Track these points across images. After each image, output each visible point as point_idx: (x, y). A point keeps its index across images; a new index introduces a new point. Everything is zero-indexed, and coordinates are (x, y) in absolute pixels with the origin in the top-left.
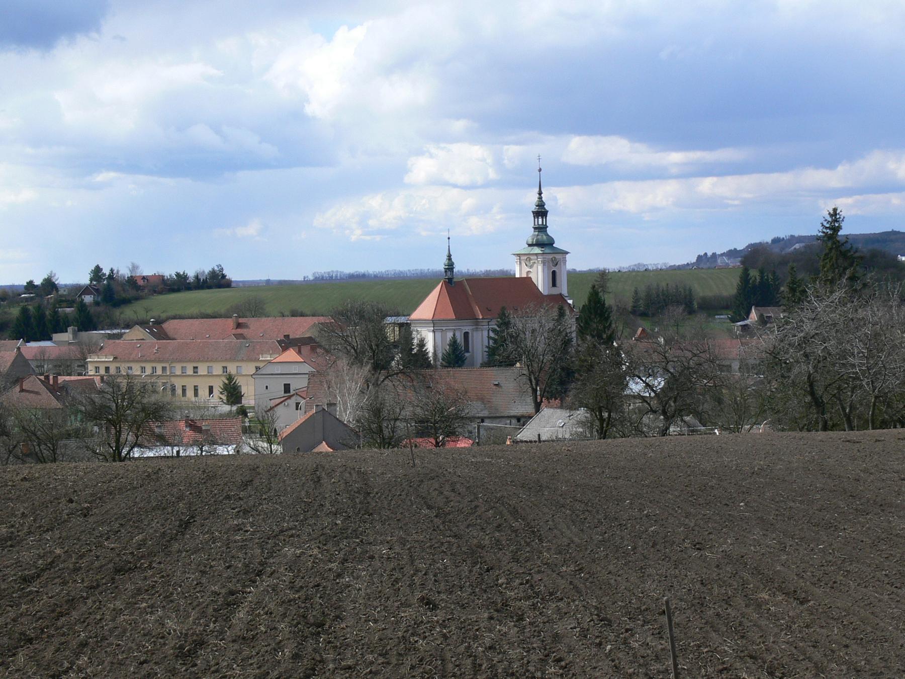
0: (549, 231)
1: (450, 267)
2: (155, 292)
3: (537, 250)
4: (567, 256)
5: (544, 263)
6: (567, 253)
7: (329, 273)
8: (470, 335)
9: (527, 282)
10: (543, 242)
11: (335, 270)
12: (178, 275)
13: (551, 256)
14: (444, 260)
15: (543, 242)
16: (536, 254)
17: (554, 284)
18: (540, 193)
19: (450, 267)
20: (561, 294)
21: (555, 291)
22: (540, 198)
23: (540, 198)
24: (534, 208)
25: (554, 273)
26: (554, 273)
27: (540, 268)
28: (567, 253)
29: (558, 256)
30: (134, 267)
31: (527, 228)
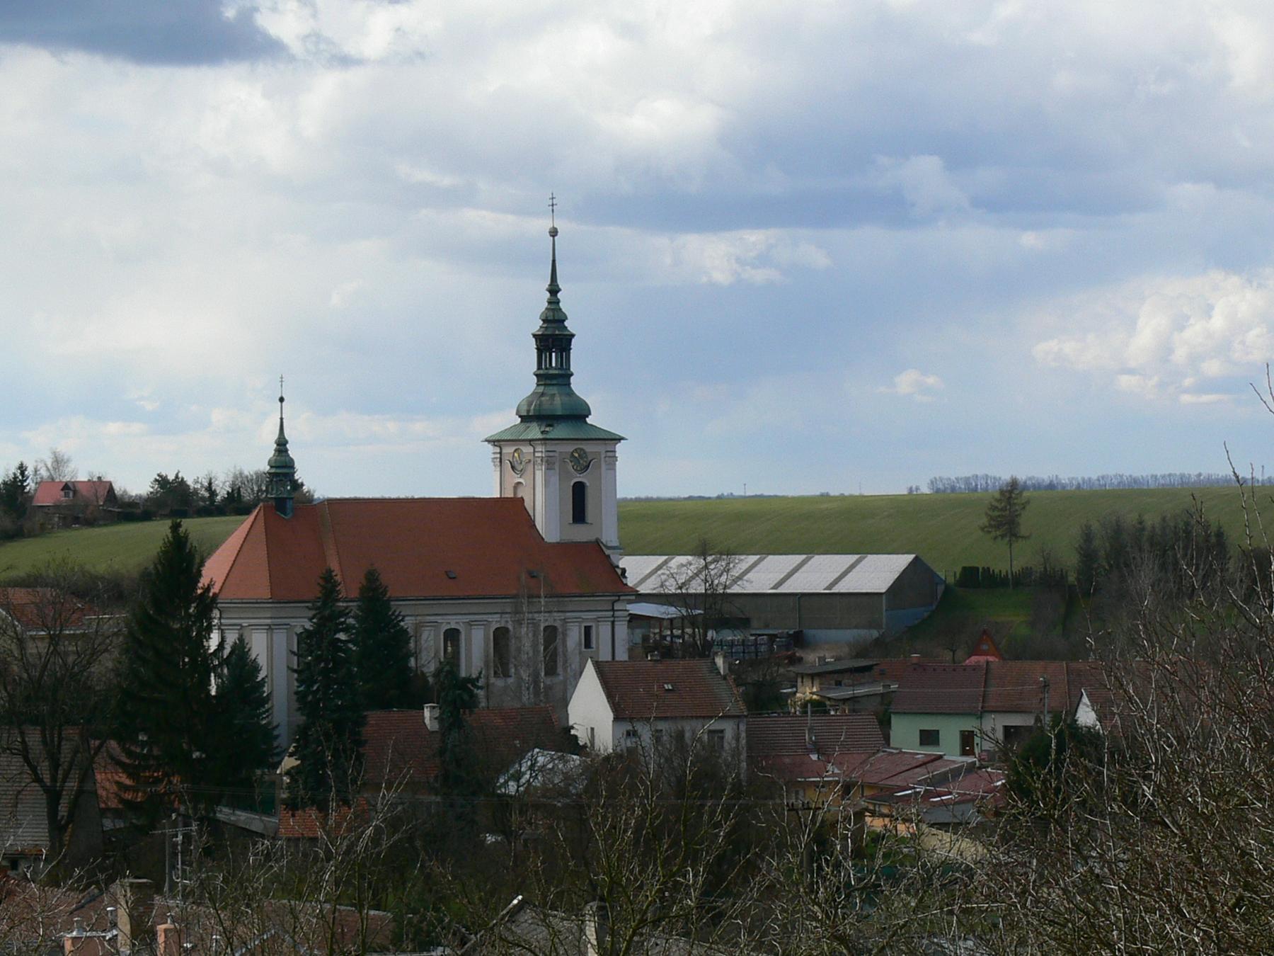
0: (577, 385)
1: (282, 467)
2: (76, 520)
3: (535, 431)
4: (620, 448)
5: (549, 463)
6: (620, 439)
7: (967, 480)
8: (463, 637)
9: (508, 512)
10: (557, 416)
11: (980, 473)
12: (162, 481)
13: (569, 448)
14: (270, 451)
15: (557, 416)
16: (530, 441)
17: (579, 515)
18: (554, 290)
19: (282, 467)
20: (597, 543)
21: (581, 534)
22: (554, 302)
23: (554, 302)
24: (536, 325)
25: (579, 491)
26: (579, 491)
27: (539, 475)
28: (620, 439)
29: (589, 448)
30: (58, 462)
31: (520, 373)
